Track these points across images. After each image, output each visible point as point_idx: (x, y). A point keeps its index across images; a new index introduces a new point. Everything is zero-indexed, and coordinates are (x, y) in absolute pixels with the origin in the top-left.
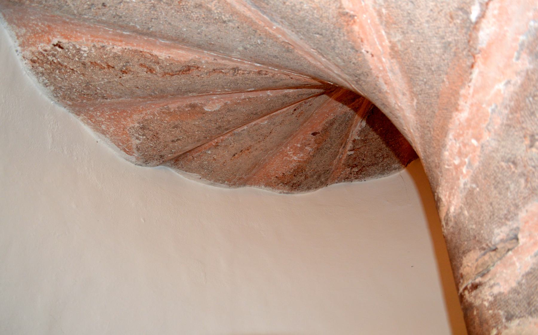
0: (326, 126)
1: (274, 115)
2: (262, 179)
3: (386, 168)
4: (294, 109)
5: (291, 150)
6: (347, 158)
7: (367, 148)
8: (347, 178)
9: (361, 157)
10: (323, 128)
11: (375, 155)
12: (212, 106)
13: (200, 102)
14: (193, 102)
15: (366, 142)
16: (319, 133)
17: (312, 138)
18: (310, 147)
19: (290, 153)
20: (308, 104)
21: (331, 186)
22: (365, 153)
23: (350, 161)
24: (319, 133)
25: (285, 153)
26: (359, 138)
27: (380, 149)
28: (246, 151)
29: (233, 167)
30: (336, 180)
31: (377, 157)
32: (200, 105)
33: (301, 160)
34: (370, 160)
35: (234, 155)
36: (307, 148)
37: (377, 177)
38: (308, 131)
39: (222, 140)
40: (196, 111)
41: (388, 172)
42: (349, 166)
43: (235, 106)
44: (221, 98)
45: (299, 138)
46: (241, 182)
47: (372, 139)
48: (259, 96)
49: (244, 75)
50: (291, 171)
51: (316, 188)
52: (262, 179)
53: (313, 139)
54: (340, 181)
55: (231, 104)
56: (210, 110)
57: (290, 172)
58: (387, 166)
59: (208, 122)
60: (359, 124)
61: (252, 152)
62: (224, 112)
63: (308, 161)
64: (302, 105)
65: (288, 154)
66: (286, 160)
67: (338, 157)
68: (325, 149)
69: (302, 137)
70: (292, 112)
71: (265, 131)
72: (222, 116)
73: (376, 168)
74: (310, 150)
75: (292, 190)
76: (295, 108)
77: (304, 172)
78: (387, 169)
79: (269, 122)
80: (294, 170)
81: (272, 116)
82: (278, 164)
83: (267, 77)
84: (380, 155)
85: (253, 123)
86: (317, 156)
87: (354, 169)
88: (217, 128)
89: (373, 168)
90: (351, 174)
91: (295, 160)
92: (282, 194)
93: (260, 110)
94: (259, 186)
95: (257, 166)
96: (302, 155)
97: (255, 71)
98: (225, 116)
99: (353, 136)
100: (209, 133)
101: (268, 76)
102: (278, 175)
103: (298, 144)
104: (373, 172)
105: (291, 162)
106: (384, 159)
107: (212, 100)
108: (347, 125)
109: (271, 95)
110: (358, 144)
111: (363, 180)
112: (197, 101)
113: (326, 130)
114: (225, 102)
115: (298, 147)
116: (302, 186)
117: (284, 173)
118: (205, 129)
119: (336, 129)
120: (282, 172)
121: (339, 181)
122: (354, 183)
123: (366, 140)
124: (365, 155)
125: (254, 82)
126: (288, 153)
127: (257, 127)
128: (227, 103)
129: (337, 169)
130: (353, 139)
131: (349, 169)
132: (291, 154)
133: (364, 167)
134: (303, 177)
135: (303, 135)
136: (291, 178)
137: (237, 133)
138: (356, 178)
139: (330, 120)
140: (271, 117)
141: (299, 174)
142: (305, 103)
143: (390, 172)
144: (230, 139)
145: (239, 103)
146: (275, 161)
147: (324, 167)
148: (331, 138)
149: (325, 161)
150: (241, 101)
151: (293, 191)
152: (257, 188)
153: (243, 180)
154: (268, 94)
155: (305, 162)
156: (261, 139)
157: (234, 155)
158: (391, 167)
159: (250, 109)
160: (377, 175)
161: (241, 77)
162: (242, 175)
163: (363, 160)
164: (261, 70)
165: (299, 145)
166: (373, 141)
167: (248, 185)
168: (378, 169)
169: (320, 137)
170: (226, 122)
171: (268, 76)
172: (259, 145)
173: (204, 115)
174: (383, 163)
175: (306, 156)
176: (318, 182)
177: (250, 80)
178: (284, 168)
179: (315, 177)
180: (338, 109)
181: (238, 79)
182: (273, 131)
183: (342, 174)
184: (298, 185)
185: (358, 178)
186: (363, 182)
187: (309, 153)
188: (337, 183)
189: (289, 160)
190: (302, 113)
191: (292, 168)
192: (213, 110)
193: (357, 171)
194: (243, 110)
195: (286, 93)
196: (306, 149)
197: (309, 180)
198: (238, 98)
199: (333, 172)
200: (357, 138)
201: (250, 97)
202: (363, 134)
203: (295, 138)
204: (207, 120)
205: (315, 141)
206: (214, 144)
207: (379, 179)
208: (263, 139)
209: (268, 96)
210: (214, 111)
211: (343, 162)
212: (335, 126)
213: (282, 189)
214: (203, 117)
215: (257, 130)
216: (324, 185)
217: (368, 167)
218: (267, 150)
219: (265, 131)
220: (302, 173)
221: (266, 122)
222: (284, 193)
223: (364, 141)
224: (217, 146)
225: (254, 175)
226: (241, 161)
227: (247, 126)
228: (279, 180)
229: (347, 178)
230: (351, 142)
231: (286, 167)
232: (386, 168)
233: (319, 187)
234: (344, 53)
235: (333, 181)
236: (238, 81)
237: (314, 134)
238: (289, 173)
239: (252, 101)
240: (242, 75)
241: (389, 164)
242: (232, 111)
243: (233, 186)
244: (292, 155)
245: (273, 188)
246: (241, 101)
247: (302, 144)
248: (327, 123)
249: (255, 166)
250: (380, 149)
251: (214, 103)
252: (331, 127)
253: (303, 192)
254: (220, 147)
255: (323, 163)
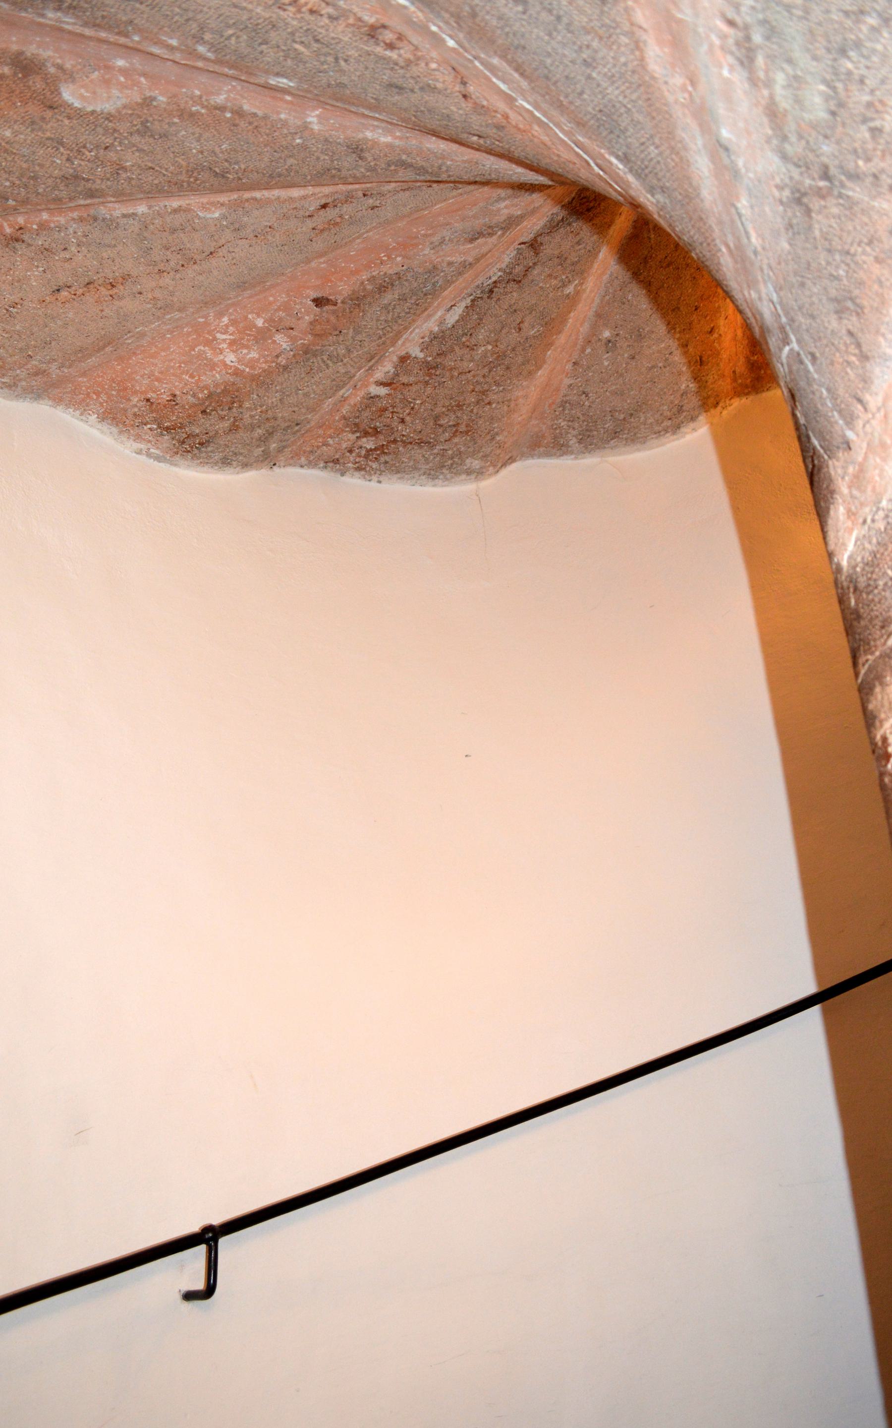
0: (365, 289)
1: (255, 199)
2: (98, 394)
3: (450, 462)
4: (323, 202)
5: (231, 329)
6: (361, 403)
7: (429, 390)
8: (336, 461)
9: (399, 410)
10: (354, 291)
11: (437, 418)
12: (94, 93)
13: (59, 61)
14: (31, 50)
15: (433, 371)
16: (335, 304)
17: (308, 313)
18: (289, 337)
19: (224, 337)
20: (371, 201)
21: (283, 470)
22: (415, 404)
23: (366, 414)
24: (335, 304)
25: (209, 333)
26: (421, 355)
27: (458, 406)
28: (102, 289)
29: (35, 329)
30: (303, 459)
31: (441, 426)
32: (52, 70)
33: (244, 371)
34: (419, 428)
35: (58, 290)
36: (279, 338)
37: (414, 480)
38: (308, 288)
39: (43, 226)
40: (29, 87)
41: (448, 476)
42: (356, 428)
43: (176, 120)
44: (144, 75)
45: (271, 299)
46: (34, 383)
47: (451, 369)
48: (275, 117)
49: (312, 18)
50: (200, 396)
51: (245, 466)
52: (98, 394)
53: (308, 313)
54: (311, 464)
55: (165, 110)
56: (77, 104)
57: (194, 395)
58: (452, 458)
59: (49, 143)
60: (439, 314)
61: (120, 298)
62: (124, 127)
63: (261, 381)
64: (352, 197)
65: (215, 339)
66: (200, 356)
67: (341, 393)
68: (325, 358)
69: (284, 298)
70: (312, 209)
71: (198, 244)
72: (109, 140)
73: (423, 456)
74: (284, 346)
75: (177, 453)
76: (330, 200)
77: (234, 410)
78: (450, 468)
79: (224, 217)
80: (210, 395)
81: (247, 200)
82: (171, 360)
83: (387, 60)
84: (451, 423)
85: (175, 203)
86: (293, 371)
87: (364, 440)
88: (64, 178)
89: (417, 453)
90: (350, 451)
91: (225, 365)
92: (143, 458)
93: (243, 167)
94: (81, 414)
95: (108, 349)
96: (254, 355)
97: (366, 18)
98: (120, 144)
99: (408, 345)
100: (26, 186)
101: (393, 55)
102: (154, 395)
103: (259, 316)
104: (411, 463)
105: (212, 366)
106: (455, 434)
107: (108, 68)
108: (417, 305)
109: (316, 127)
110: (408, 373)
111: (375, 478)
112: (50, 53)
113: (358, 300)
114: (148, 95)
115: (255, 326)
116: (209, 449)
117: (175, 396)
118: (25, 165)
119: (386, 307)
120: (170, 390)
121: (310, 462)
122: (347, 479)
123: (436, 368)
124: (412, 408)
125: (322, 59)
126: (219, 336)
127: (179, 219)
128: (153, 99)
129: (320, 427)
130: (403, 353)
131: (352, 437)
132: (224, 340)
133: (395, 441)
134: (226, 424)
135: (288, 295)
136: (189, 416)
137: (104, 219)
138: (359, 469)
139: (385, 273)
140: (238, 205)
141: (220, 412)
142: (364, 195)
143: (452, 478)
144: (71, 230)
145: (192, 115)
146: (169, 348)
147: (296, 409)
148: (357, 332)
149: (306, 395)
150: (203, 111)
151: (177, 458)
152: (73, 416)
153: (45, 379)
154: (309, 119)
155: (254, 378)
156: (172, 263)
157: (58, 290)
158: (463, 462)
159: (217, 150)
160: (416, 475)
161: (295, 23)
162: (49, 362)
163: (403, 421)
164: (387, 24)
165: (260, 323)
166: (452, 377)
167: (46, 401)
168: (427, 460)
169: (333, 319)
170: (108, 169)
171: (393, 55)
172: (154, 284)
173: (49, 114)
174: (446, 447)
175: (266, 362)
176: (258, 451)
177: (316, 46)
178: (181, 380)
179: (259, 431)
180: (423, 250)
181: (281, 24)
182: (222, 252)
183: (327, 445)
184: (201, 444)
185: (364, 469)
186: (373, 484)
187: (277, 356)
188: (302, 466)
189: (211, 360)
190: (336, 224)
191: (206, 387)
192: (90, 109)
193: (371, 450)
194: (195, 144)
195: (366, 139)
196: (274, 342)
197: (238, 436)
198: (200, 97)
199: (306, 432)
200: (416, 352)
201: (246, 107)
202: (435, 349)
203: (261, 296)
204: (48, 134)
205: (311, 323)
206: (8, 230)
207: (418, 489)
208: (179, 267)
209: (306, 127)
210: (93, 112)
211: (345, 410)
212: (388, 297)
213: (150, 441)
214: (43, 119)
215: (174, 231)
216: (266, 462)
217: (404, 447)
218: (168, 307)
219: (198, 244)
220: (230, 409)
221: (217, 215)
222: (149, 455)
223: (429, 368)
224: (17, 240)
225: (84, 374)
226: (71, 315)
227: (150, 207)
228: (152, 412)
229: (334, 463)
230: (395, 359)
231: (192, 376)
232: (450, 462)
233: (255, 464)
234: (870, 82)
235: (294, 460)
236: (273, 34)
237: (319, 302)
238: (192, 400)
239: (243, 124)
240: (308, 16)
241: (460, 453)
242: (152, 136)
243: (6, 390)
244: (225, 346)
245: (121, 432)
246: (203, 111)
247: (270, 321)
248: (372, 279)
249: (104, 347)
250: (458, 406)
251: (107, 83)
252: (377, 296)
253: (206, 468)
254: (24, 246)
255: (301, 396)
